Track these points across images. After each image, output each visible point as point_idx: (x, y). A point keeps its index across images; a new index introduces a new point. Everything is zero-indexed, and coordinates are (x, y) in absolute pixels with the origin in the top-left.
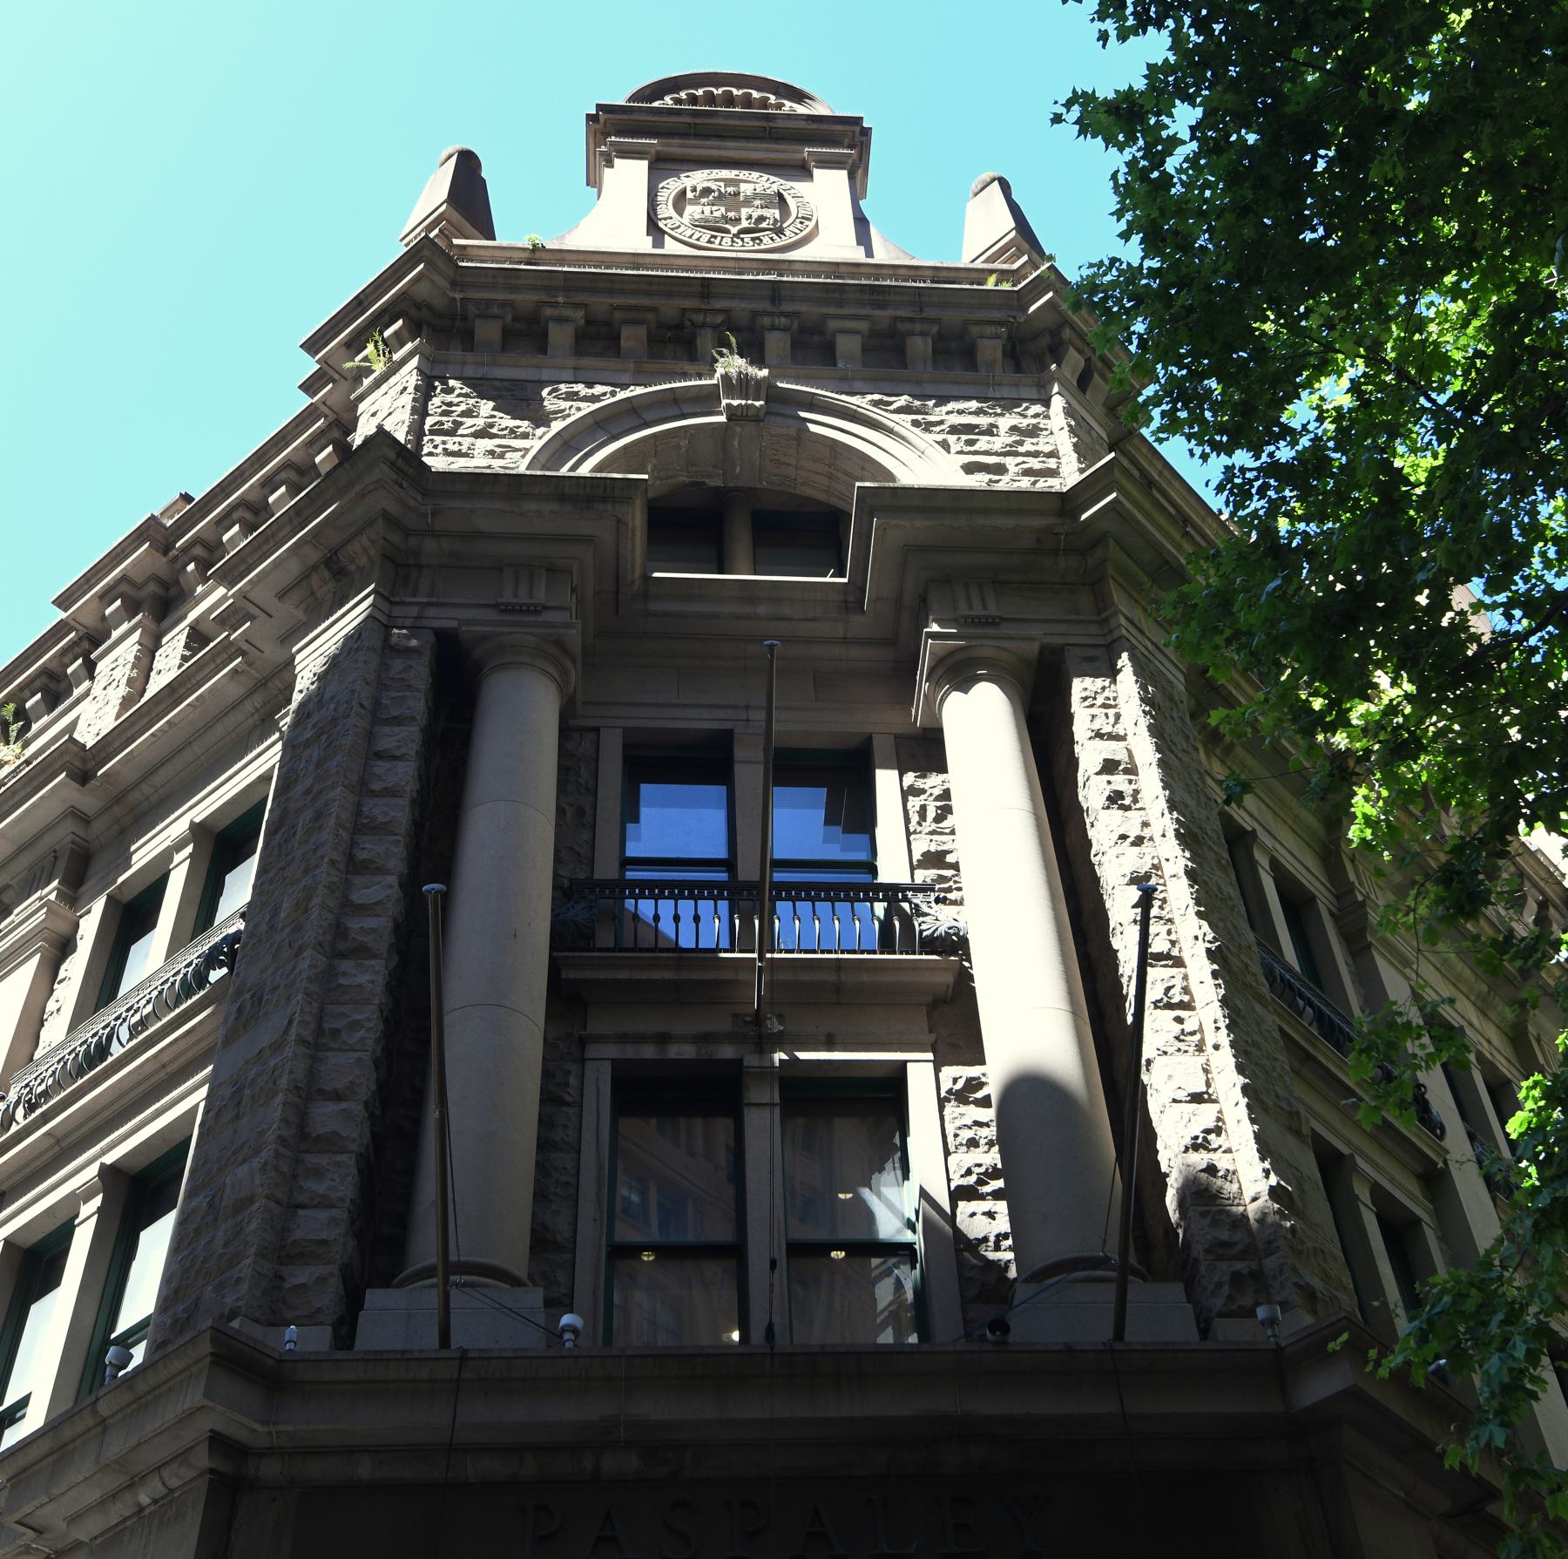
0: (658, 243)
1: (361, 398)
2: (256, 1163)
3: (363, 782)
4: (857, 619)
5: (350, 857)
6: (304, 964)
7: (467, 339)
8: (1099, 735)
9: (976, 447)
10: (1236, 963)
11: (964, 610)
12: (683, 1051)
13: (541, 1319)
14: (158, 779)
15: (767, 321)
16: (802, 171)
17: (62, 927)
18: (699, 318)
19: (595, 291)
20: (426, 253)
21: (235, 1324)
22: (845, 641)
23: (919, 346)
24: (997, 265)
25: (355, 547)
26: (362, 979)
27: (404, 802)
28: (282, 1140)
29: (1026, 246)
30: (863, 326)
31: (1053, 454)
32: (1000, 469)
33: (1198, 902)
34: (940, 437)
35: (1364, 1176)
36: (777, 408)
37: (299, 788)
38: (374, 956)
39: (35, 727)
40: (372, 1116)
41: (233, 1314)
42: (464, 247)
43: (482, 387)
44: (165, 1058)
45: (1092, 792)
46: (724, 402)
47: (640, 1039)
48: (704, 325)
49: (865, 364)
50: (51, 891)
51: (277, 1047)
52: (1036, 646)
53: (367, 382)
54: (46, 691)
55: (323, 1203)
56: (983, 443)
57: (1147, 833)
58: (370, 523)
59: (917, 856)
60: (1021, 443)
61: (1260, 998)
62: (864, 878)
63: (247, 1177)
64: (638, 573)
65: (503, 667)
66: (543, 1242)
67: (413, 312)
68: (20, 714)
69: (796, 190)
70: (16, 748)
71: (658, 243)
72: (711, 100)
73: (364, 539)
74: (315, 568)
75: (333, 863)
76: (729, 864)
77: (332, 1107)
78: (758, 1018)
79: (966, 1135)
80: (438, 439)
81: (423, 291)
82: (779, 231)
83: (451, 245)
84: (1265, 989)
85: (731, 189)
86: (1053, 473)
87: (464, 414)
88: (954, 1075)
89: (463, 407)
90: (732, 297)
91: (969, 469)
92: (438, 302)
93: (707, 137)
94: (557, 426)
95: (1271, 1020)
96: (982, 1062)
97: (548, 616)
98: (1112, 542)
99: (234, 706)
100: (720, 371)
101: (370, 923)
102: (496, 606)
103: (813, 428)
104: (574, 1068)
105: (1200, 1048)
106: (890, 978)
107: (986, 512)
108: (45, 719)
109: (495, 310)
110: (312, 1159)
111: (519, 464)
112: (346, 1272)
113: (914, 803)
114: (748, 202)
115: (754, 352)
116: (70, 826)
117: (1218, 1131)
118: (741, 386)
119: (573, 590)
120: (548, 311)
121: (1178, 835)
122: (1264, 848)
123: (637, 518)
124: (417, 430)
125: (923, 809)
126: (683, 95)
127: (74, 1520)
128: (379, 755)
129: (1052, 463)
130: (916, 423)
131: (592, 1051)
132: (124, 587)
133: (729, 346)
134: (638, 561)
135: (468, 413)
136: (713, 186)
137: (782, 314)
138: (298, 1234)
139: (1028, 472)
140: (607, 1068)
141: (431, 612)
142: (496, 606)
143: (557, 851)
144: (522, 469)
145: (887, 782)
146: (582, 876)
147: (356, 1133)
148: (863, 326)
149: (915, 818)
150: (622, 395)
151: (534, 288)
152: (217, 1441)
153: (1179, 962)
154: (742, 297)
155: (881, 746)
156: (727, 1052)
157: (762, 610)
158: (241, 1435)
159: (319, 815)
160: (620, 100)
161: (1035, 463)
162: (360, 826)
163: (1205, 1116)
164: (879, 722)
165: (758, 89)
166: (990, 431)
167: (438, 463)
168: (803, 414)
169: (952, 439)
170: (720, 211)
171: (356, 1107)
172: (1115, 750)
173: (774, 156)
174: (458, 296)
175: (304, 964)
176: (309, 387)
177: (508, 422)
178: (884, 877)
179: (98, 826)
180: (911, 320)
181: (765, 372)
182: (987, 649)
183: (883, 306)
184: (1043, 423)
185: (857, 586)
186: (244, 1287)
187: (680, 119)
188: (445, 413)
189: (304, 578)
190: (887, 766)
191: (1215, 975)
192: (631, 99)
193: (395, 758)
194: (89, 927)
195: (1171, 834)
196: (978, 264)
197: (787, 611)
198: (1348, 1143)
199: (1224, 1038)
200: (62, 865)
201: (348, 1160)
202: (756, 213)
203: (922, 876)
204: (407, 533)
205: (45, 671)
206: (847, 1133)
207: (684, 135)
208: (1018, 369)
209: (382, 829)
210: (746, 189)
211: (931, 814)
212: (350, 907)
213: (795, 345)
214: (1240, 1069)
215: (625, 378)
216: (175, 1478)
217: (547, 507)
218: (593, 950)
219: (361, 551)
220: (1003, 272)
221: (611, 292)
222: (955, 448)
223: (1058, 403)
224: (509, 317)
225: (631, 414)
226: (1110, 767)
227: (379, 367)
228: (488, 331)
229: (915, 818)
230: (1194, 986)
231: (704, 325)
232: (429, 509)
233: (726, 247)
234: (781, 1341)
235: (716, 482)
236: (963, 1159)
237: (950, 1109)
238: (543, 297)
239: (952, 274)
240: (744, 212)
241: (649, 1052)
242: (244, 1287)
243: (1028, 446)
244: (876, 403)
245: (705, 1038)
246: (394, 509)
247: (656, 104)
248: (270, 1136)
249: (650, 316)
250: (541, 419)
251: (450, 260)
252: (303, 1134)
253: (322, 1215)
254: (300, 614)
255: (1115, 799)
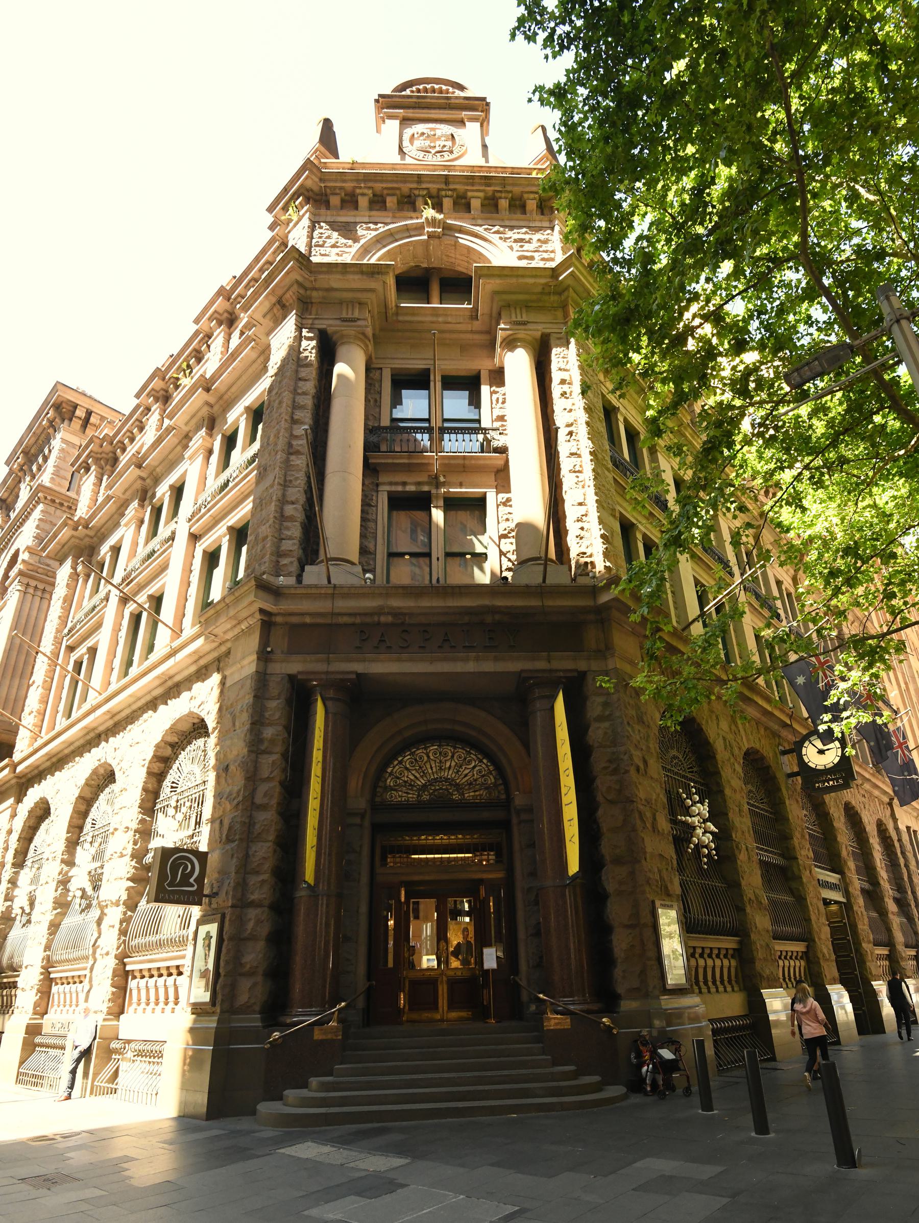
0: (403, 158)
1: (289, 232)
2: (268, 525)
3: (295, 390)
4: (476, 323)
5: (292, 418)
6: (278, 457)
7: (327, 205)
8: (560, 369)
9: (524, 248)
10: (600, 456)
11: (514, 319)
12: (411, 488)
13: (362, 576)
14: (233, 390)
15: (443, 193)
16: (461, 123)
17: (209, 445)
18: (417, 192)
19: (376, 181)
20: (309, 166)
21: (265, 576)
22: (472, 332)
23: (504, 203)
24: (539, 166)
25: (287, 296)
26: (298, 462)
27: (310, 397)
28: (275, 517)
29: (550, 157)
30: (481, 194)
31: (553, 252)
32: (532, 258)
33: (589, 434)
34: (509, 244)
35: (640, 531)
36: (447, 232)
37: (274, 392)
38: (303, 454)
39: (194, 371)
40: (305, 510)
41: (264, 573)
42: (325, 163)
43: (333, 226)
44: (242, 490)
45: (556, 390)
46: (426, 229)
47: (396, 484)
48: (419, 196)
49: (482, 212)
50: (203, 432)
51: (272, 486)
52: (539, 333)
53: (291, 225)
54: (195, 357)
55: (290, 538)
56: (527, 246)
57: (573, 408)
58: (292, 285)
59: (494, 417)
60: (541, 246)
61: (608, 469)
62: (476, 425)
63: (265, 530)
64: (394, 304)
65: (343, 343)
66: (364, 551)
67: (306, 193)
68: (189, 366)
69: (457, 132)
70: (189, 379)
71: (403, 158)
72: (426, 90)
73: (291, 293)
74: (274, 304)
75: (286, 420)
76: (428, 420)
77: (291, 507)
78: (436, 477)
79: (505, 517)
80: (317, 249)
81: (309, 183)
82: (451, 152)
83: (321, 162)
84: (610, 465)
85: (432, 133)
86: (552, 260)
87: (327, 238)
88: (503, 497)
89: (326, 235)
90: (430, 182)
91: (520, 258)
92: (316, 189)
93: (423, 108)
94: (362, 242)
95: (610, 476)
96: (510, 492)
97: (360, 323)
98: (571, 289)
99: (254, 362)
100: (425, 216)
101: (300, 442)
102: (340, 319)
103: (460, 240)
104: (375, 494)
105: (583, 487)
106: (482, 462)
107: (523, 276)
108: (197, 368)
109: (338, 191)
110: (285, 524)
111: (347, 259)
112: (299, 560)
113: (495, 397)
114: (439, 138)
115: (438, 207)
116: (206, 408)
117: (586, 515)
118: (433, 222)
119: (369, 312)
120: (358, 191)
121: (585, 408)
122: (622, 414)
123: (391, 281)
124: (309, 245)
125: (498, 399)
126: (414, 88)
127: (225, 633)
128: (300, 379)
129: (552, 255)
130: (501, 238)
131: (380, 488)
132: (216, 315)
133: (427, 204)
134: (393, 299)
135: (329, 237)
136: (425, 131)
137: (450, 190)
138: (283, 548)
139: (543, 259)
140: (386, 494)
141: (316, 322)
142: (340, 319)
143: (365, 416)
144: (349, 261)
145: (485, 390)
146: (376, 425)
147: (300, 516)
148: (481, 194)
149: (494, 402)
150: (387, 228)
151: (352, 181)
152: (262, 611)
153: (579, 456)
154: (433, 182)
155: (484, 376)
156: (426, 488)
157: (440, 319)
158: (269, 609)
159: (280, 403)
160: (388, 91)
161: (545, 255)
162: (295, 406)
163: (582, 510)
164: (484, 365)
165: (446, 85)
166: (529, 242)
167: (314, 259)
168: (457, 235)
169: (514, 245)
170: (427, 143)
171: (299, 507)
172: (565, 376)
173: (450, 116)
174: (323, 185)
175: (278, 457)
176: (272, 227)
177: (343, 240)
178: (483, 426)
179: (216, 408)
180: (501, 192)
181: (442, 216)
182: (521, 334)
183: (489, 185)
184: (550, 237)
185: (475, 309)
186: (267, 564)
187: (410, 100)
188: (320, 237)
189: (271, 309)
190: (486, 384)
191: (591, 460)
192: (394, 91)
193: (306, 380)
194: (217, 445)
195: (582, 408)
196: (531, 166)
197: (450, 319)
198: (637, 520)
199: (592, 483)
200: (206, 422)
201: (298, 524)
202: (442, 143)
203: (497, 424)
204: (306, 289)
205: (195, 350)
206: (463, 516)
207: (414, 108)
208: (542, 214)
209: (302, 407)
210: (438, 133)
211: (500, 401)
212: (293, 436)
213: (455, 203)
214: (596, 494)
215: (388, 220)
216: (251, 621)
217: (357, 277)
218: (379, 452)
219: (290, 297)
220: (540, 169)
221: (381, 181)
222: (515, 249)
223: (557, 228)
224: (343, 194)
225: (391, 236)
226: (563, 382)
227: (295, 218)
228: (335, 200)
229: (494, 402)
230: (584, 465)
231: (419, 196)
232: (313, 279)
233: (431, 160)
234: (442, 581)
235: (425, 265)
236: (504, 525)
237: (501, 508)
238: (355, 184)
239: (519, 171)
240: (438, 143)
241: (400, 488)
242: (267, 564)
243: (544, 247)
244: (485, 229)
245: (419, 484)
246: (300, 279)
247: (403, 93)
248: (272, 516)
249: (398, 192)
250: (356, 240)
251: (319, 169)
252: (282, 516)
253: (290, 542)
254: (271, 324)
255: (563, 394)
